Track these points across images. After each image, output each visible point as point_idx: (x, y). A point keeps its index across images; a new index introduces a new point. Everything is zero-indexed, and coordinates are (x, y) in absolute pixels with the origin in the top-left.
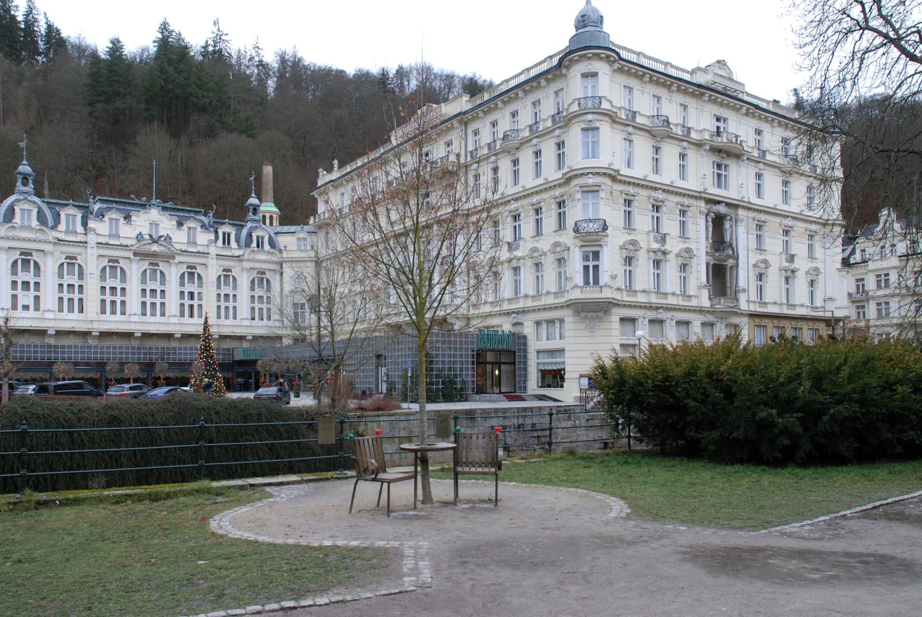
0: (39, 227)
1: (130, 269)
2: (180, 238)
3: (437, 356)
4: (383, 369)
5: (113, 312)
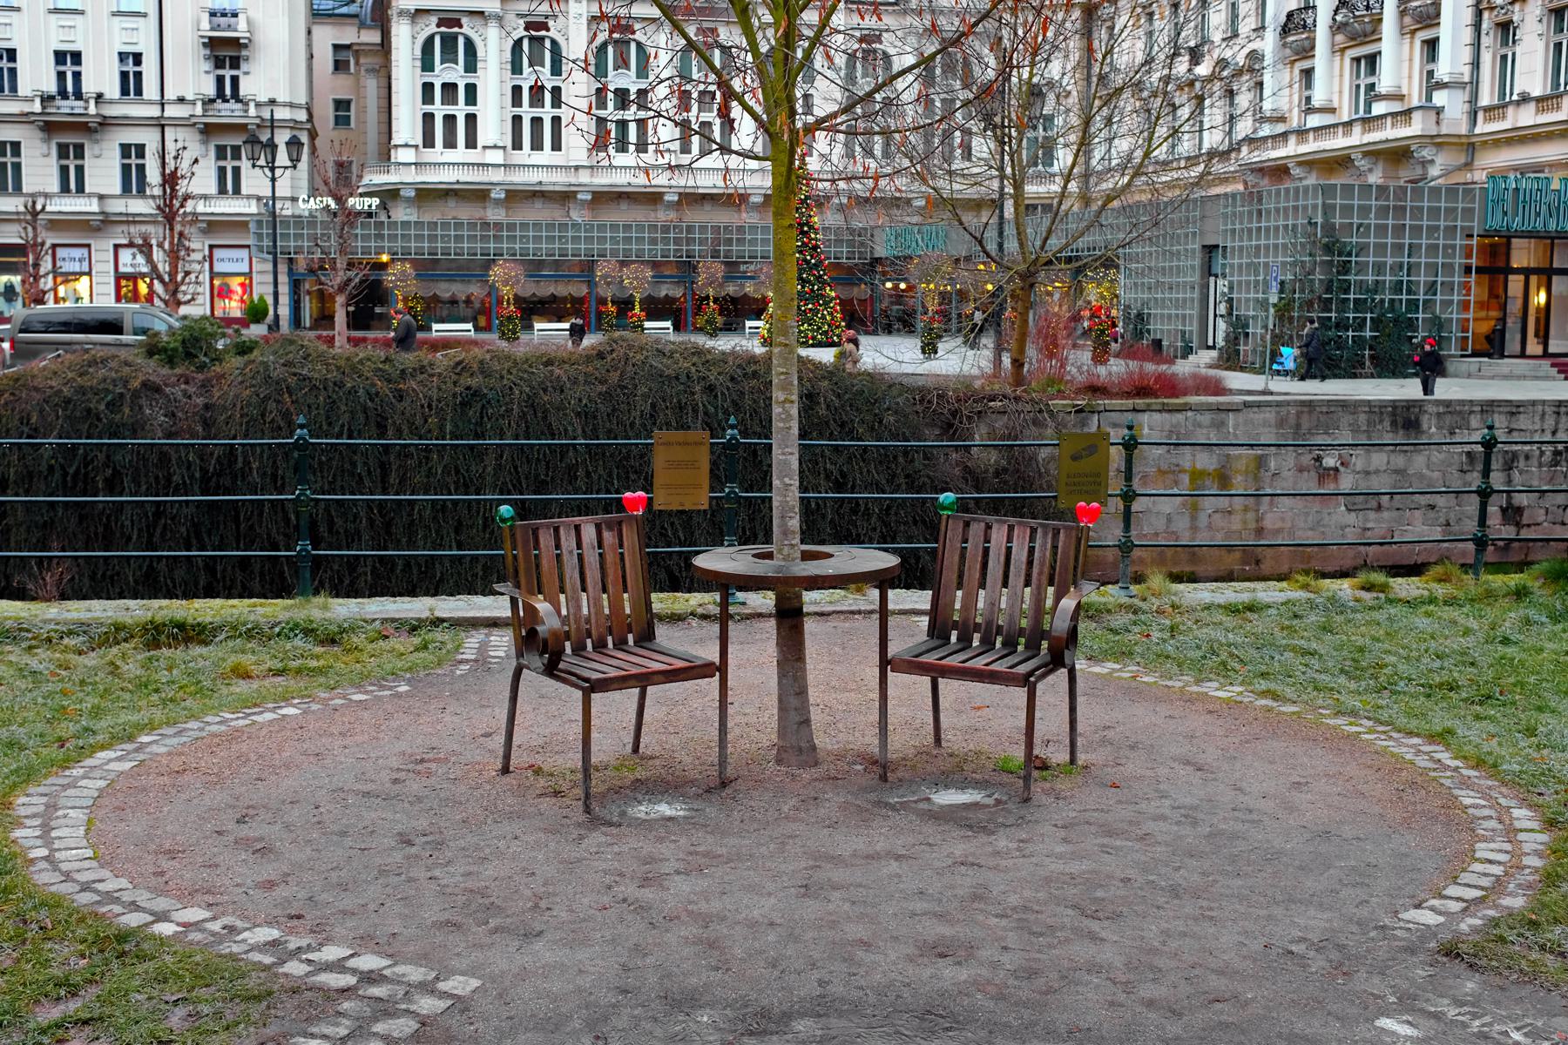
3: (1362, 249)
4: (1220, 282)
5: (537, 145)
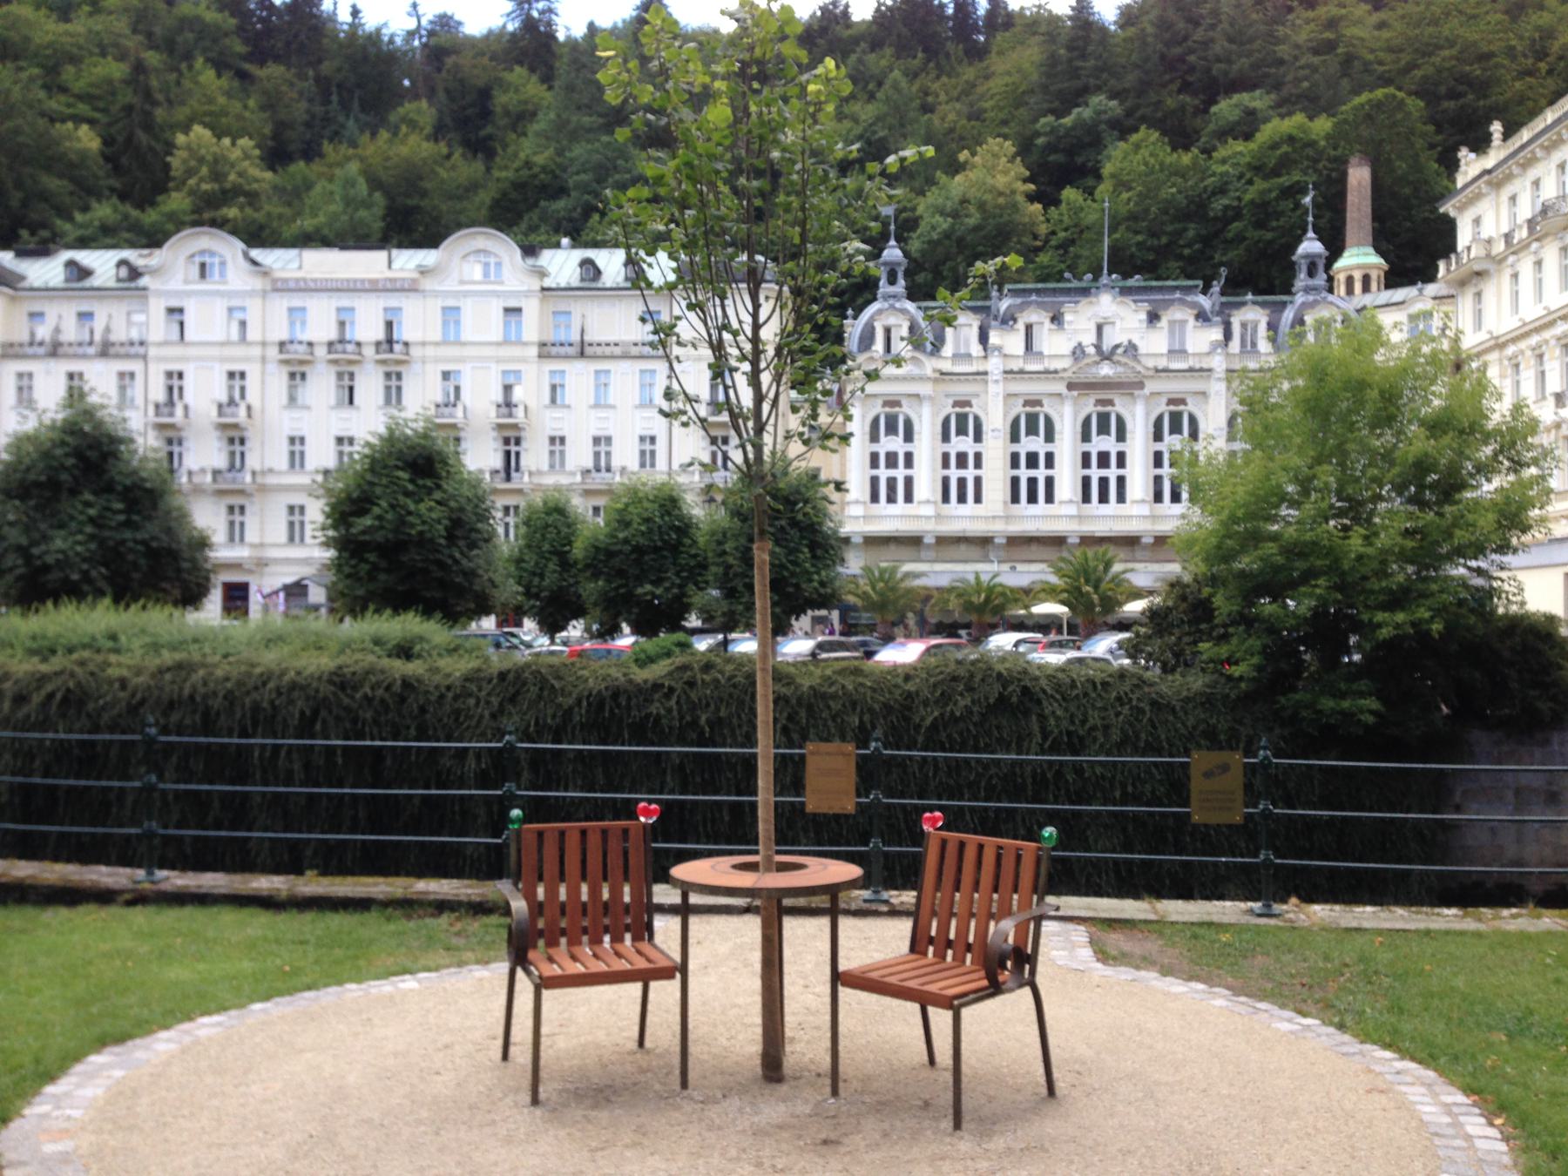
0: (909, 355)
2: (1154, 343)
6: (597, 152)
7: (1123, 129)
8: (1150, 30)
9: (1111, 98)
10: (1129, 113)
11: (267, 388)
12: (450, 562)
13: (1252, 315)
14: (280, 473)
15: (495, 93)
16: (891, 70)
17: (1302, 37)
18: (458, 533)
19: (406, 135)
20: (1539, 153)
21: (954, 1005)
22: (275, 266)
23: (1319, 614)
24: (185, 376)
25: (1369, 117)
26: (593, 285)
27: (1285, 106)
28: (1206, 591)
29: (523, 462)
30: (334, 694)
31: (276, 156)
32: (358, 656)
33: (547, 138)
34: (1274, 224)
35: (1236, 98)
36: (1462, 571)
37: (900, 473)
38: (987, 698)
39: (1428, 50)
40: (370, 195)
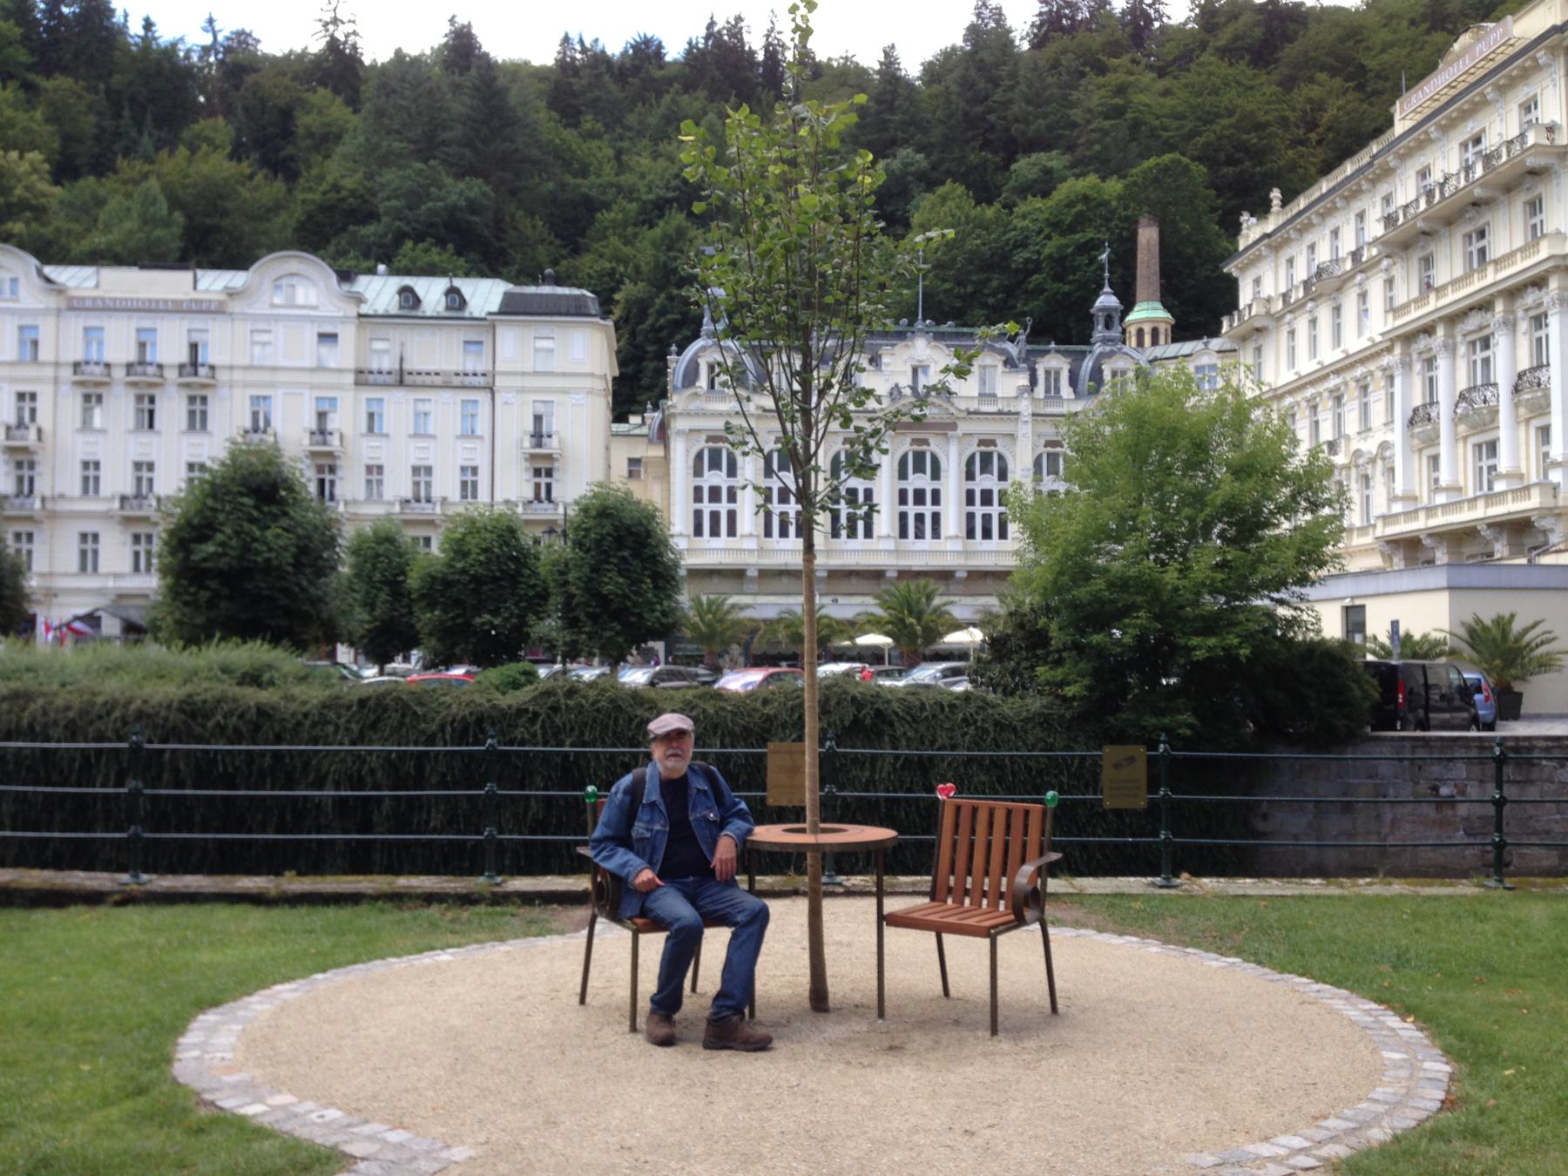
1: (947, 455)
6: (409, 177)
7: (930, 182)
8: (954, 88)
9: (918, 151)
10: (934, 168)
11: (59, 411)
12: (296, 589)
13: (1055, 362)
14: (72, 499)
15: (297, 113)
16: (705, 113)
17: (1095, 101)
18: (304, 560)
19: (207, 154)
20: (1315, 220)
21: (991, 934)
22: (71, 284)
23: (1141, 639)
24: (39, 398)
25: (1156, 180)
26: (413, 313)
27: (1080, 167)
28: (1042, 621)
29: (338, 491)
30: (185, 722)
31: (64, 171)
32: (206, 685)
33: (355, 162)
34: (1071, 277)
35: (1034, 156)
36: (1267, 602)
37: (723, 507)
38: (842, 721)
39: (1209, 118)
40: (170, 213)
